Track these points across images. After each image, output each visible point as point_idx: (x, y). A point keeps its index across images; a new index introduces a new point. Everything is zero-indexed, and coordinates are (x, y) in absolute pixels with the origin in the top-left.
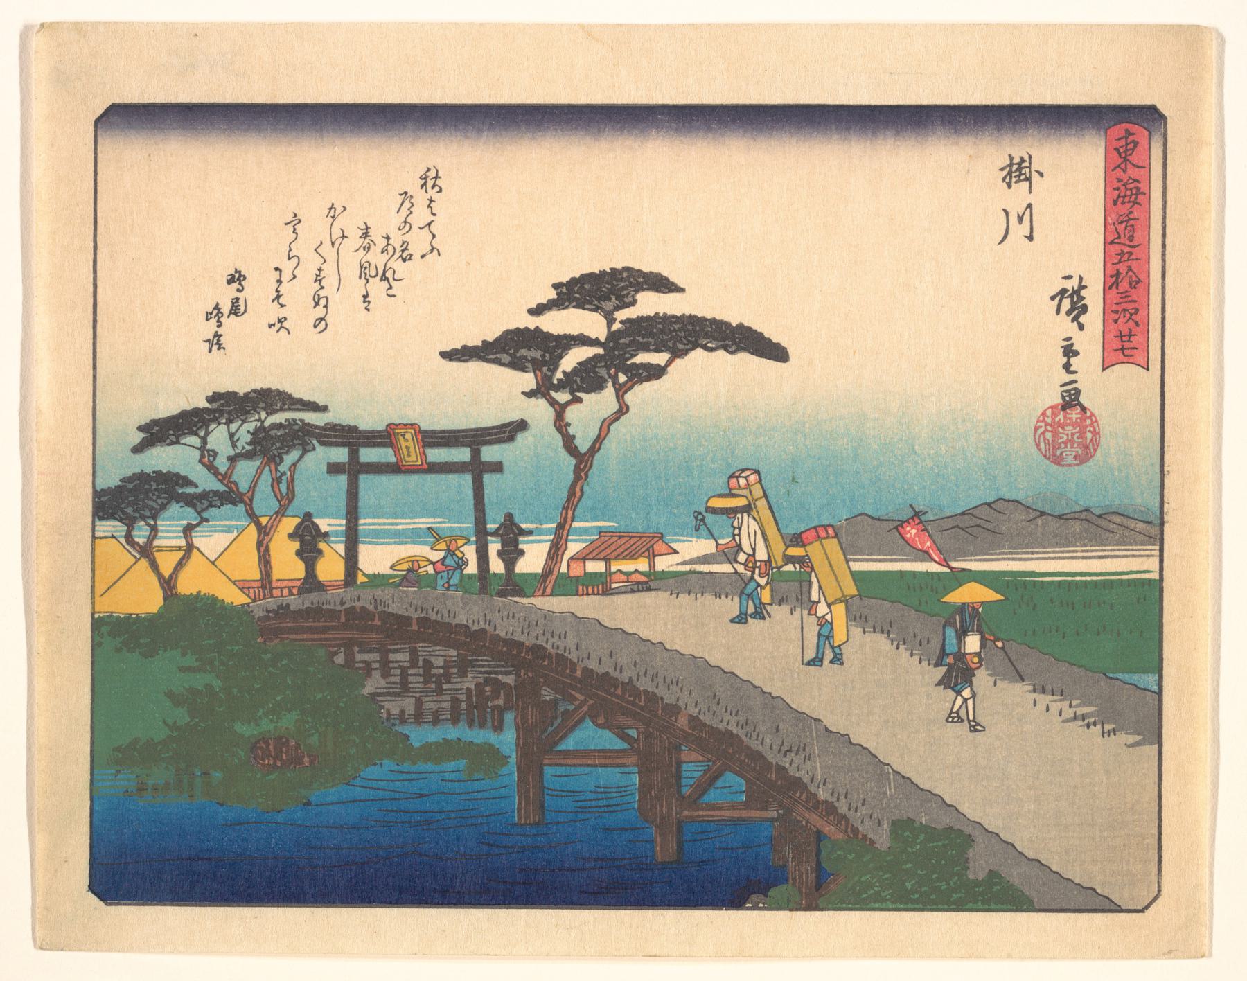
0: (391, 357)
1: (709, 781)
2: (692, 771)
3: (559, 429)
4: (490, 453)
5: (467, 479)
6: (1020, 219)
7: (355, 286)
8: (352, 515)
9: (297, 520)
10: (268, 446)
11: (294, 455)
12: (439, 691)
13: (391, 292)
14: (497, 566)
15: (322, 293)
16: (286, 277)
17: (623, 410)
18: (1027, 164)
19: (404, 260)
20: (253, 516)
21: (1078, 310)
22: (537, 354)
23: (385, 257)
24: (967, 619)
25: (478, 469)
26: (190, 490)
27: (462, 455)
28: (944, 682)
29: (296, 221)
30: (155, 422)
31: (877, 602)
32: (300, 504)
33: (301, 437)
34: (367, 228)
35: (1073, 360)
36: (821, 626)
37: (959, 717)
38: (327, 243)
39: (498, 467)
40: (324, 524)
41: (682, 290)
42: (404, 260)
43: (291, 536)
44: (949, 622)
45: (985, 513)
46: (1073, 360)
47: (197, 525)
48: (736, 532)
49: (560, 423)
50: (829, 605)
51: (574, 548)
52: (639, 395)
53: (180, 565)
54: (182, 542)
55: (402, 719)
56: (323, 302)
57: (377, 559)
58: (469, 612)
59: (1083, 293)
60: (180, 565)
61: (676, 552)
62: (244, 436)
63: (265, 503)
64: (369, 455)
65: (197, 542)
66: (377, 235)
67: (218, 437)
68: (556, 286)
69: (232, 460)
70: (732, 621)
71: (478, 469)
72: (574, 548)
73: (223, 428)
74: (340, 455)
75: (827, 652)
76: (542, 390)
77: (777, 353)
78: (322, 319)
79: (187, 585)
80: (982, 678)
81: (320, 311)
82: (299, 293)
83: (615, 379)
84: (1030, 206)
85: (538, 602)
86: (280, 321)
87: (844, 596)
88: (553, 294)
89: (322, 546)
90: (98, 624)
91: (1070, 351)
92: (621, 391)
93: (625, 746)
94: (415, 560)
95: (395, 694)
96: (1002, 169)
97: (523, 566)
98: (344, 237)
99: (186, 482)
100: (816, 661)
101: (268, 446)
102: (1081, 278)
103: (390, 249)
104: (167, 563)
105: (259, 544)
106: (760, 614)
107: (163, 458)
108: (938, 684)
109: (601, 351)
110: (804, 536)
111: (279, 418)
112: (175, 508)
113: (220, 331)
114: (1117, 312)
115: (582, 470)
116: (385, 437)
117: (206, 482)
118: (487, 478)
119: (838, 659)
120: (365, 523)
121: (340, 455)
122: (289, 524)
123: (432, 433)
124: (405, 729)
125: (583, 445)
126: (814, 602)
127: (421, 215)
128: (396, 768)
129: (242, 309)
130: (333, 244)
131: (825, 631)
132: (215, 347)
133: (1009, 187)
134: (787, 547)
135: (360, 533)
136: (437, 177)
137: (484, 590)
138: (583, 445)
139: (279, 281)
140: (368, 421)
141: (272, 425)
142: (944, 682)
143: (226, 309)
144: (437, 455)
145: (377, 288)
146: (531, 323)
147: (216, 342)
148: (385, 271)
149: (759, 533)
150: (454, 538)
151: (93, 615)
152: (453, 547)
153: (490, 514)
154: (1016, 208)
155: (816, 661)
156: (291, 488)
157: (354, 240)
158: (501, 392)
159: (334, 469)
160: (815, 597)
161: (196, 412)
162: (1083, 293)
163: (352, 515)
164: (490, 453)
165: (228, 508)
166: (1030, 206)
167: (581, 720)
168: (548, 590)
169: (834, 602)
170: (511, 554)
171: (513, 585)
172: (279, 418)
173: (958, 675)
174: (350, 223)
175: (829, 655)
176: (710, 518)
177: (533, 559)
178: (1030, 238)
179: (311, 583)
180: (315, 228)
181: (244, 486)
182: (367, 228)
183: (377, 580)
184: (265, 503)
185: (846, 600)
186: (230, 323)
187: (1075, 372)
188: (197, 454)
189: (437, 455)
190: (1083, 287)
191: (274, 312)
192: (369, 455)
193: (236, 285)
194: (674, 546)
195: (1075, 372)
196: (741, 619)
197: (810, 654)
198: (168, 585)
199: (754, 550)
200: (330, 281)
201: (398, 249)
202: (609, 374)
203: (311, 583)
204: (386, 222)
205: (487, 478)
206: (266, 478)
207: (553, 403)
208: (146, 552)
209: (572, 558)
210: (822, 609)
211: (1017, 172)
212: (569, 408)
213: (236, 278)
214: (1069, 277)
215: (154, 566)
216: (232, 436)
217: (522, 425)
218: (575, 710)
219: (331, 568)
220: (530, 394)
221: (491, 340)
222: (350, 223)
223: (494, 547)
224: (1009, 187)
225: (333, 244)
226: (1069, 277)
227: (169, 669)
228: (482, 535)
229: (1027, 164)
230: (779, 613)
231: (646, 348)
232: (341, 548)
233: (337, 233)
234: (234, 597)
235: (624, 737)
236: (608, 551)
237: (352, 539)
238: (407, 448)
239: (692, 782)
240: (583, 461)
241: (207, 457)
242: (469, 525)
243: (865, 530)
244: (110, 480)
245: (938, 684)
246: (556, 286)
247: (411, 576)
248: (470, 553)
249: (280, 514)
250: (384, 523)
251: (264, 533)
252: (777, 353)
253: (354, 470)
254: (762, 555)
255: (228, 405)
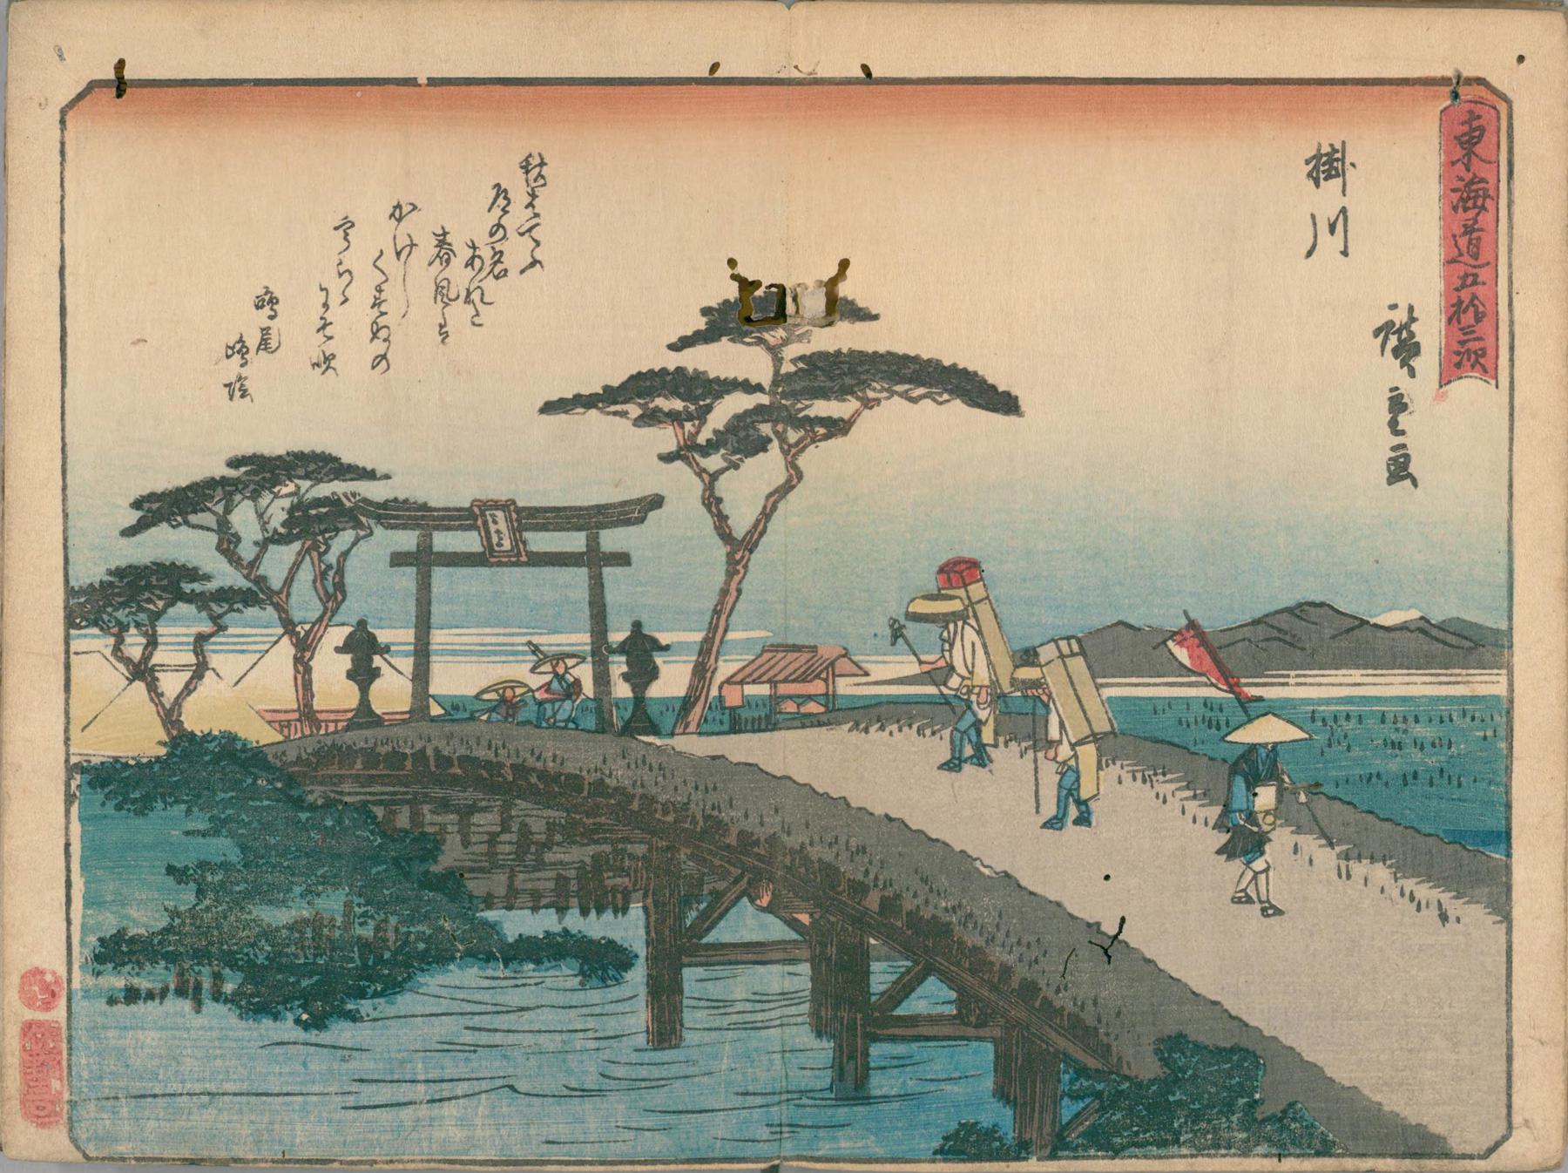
0: (465, 411)
1: (903, 988)
2: (881, 976)
3: (708, 506)
4: (611, 539)
5: (581, 575)
6: (1332, 229)
7: (426, 312)
8: (423, 625)
9: (348, 630)
10: (310, 525)
11: (347, 536)
12: (540, 865)
13: (477, 320)
14: (622, 690)
15: (382, 321)
16: (335, 300)
17: (795, 476)
18: (1338, 155)
19: (497, 277)
20: (289, 626)
21: (1407, 351)
22: (678, 405)
23: (469, 272)
24: (1256, 766)
25: (595, 560)
26: (197, 587)
27: (575, 542)
28: (1228, 851)
29: (346, 226)
30: (152, 497)
31: (1141, 742)
32: (352, 609)
33: (340, 514)
34: (445, 234)
35: (1402, 418)
36: (1063, 775)
37: (1247, 895)
38: (390, 254)
39: (623, 559)
40: (383, 636)
41: (876, 317)
42: (497, 277)
43: (338, 650)
44: (1234, 770)
45: (1284, 621)
46: (1402, 418)
47: (212, 635)
48: (947, 646)
49: (712, 502)
50: (1073, 746)
51: (725, 669)
52: (819, 458)
53: (188, 689)
54: (191, 659)
55: (489, 902)
56: (383, 334)
57: (456, 679)
58: (584, 756)
59: (1414, 327)
60: (188, 689)
61: (867, 674)
62: (278, 514)
63: (305, 602)
64: (444, 541)
65: (215, 660)
66: (457, 241)
67: (244, 518)
68: (706, 311)
69: (263, 545)
70: (940, 767)
71: (595, 560)
72: (725, 669)
73: (248, 503)
74: (407, 540)
75: (1074, 808)
76: (684, 453)
77: (1006, 404)
78: (384, 357)
79: (198, 717)
80: (1281, 840)
81: (379, 347)
82: (353, 319)
83: (782, 439)
84: (1344, 211)
85: (682, 743)
86: (326, 359)
87: (1094, 734)
88: (701, 323)
89: (377, 661)
90: (71, 769)
91: (1398, 404)
92: (791, 453)
93: (794, 936)
94: (514, 684)
95: (482, 870)
96: (1307, 162)
97: (655, 691)
98: (413, 245)
99: (193, 574)
100: (1055, 823)
101: (310, 525)
102: (1411, 309)
103: (477, 262)
104: (171, 684)
105: (297, 660)
106: (981, 757)
107: (184, 544)
108: (1219, 852)
109: (764, 399)
110: (726, 727)
111: (325, 490)
112: (182, 608)
113: (244, 372)
114: (1458, 353)
115: (738, 562)
116: (469, 517)
117: (226, 575)
118: (608, 572)
119: (1084, 820)
120: (438, 637)
121: (407, 540)
122: (336, 635)
123: (533, 512)
124: (491, 915)
125: (741, 523)
126: (1052, 742)
127: (518, 216)
128: (481, 973)
129: (274, 344)
130: (398, 254)
131: (1069, 780)
132: (238, 394)
133: (1318, 186)
134: (1016, 667)
135: (433, 647)
136: (542, 164)
137: (604, 727)
138: (741, 523)
139: (326, 305)
140: (437, 496)
141: (315, 497)
142: (1228, 851)
143: (253, 341)
144: (540, 542)
145: (459, 314)
146: (672, 361)
147: (238, 389)
148: (469, 293)
149: (979, 647)
150: (561, 657)
151: (67, 761)
152: (561, 670)
153: (612, 619)
154: (1328, 211)
155: (1055, 823)
156: (340, 586)
157: (428, 247)
158: (623, 457)
159: (398, 560)
160: (1054, 733)
161: (212, 483)
162: (1414, 327)
163: (423, 625)
164: (611, 539)
165: (252, 612)
166: (1344, 211)
167: (738, 898)
168: (692, 728)
169: (1081, 742)
170: (642, 673)
171: (642, 719)
172: (325, 490)
173: (1244, 842)
174: (421, 229)
175: (1073, 812)
176: (912, 630)
177: (672, 680)
178: (1345, 253)
179: (365, 715)
180: (374, 233)
181: (276, 583)
182: (445, 234)
183: (455, 708)
184: (305, 602)
185: (1095, 737)
186: (259, 361)
187: (1403, 433)
188: (213, 538)
189: (540, 542)
190: (1413, 320)
191: (313, 346)
192: (444, 541)
193: (267, 311)
194: (866, 666)
195: (1403, 433)
196: (953, 765)
197: (1049, 809)
198: (170, 717)
199: (971, 673)
200: (393, 306)
201: (488, 262)
202: (776, 433)
203: (365, 715)
204: (470, 226)
205: (608, 572)
206: (306, 574)
207: (701, 472)
208: (142, 672)
209: (728, 681)
210: (1065, 751)
211: (1327, 166)
212: (722, 477)
213: (267, 301)
214: (1394, 307)
215: (152, 687)
216: (260, 516)
217: (657, 502)
218: (728, 889)
219: (392, 690)
220: (667, 458)
221: (616, 383)
222: (421, 229)
223: (618, 665)
224: (1318, 186)
225: (398, 254)
226: (1394, 307)
227: (173, 828)
228: (600, 653)
229: (1338, 155)
230: (1007, 758)
231: (824, 394)
232: (407, 664)
233: (403, 241)
234: (261, 734)
235: (793, 924)
236: (771, 673)
237: (422, 653)
238: (498, 532)
239: (882, 988)
240: (740, 548)
241: (228, 544)
242: (581, 640)
243: (1115, 647)
244: (91, 571)
245: (1219, 852)
246: (706, 311)
247: (506, 703)
248: (584, 673)
249: (327, 616)
250: (468, 637)
251: (304, 648)
252: (1006, 404)
253: (423, 560)
254: (982, 675)
255: (262, 471)
